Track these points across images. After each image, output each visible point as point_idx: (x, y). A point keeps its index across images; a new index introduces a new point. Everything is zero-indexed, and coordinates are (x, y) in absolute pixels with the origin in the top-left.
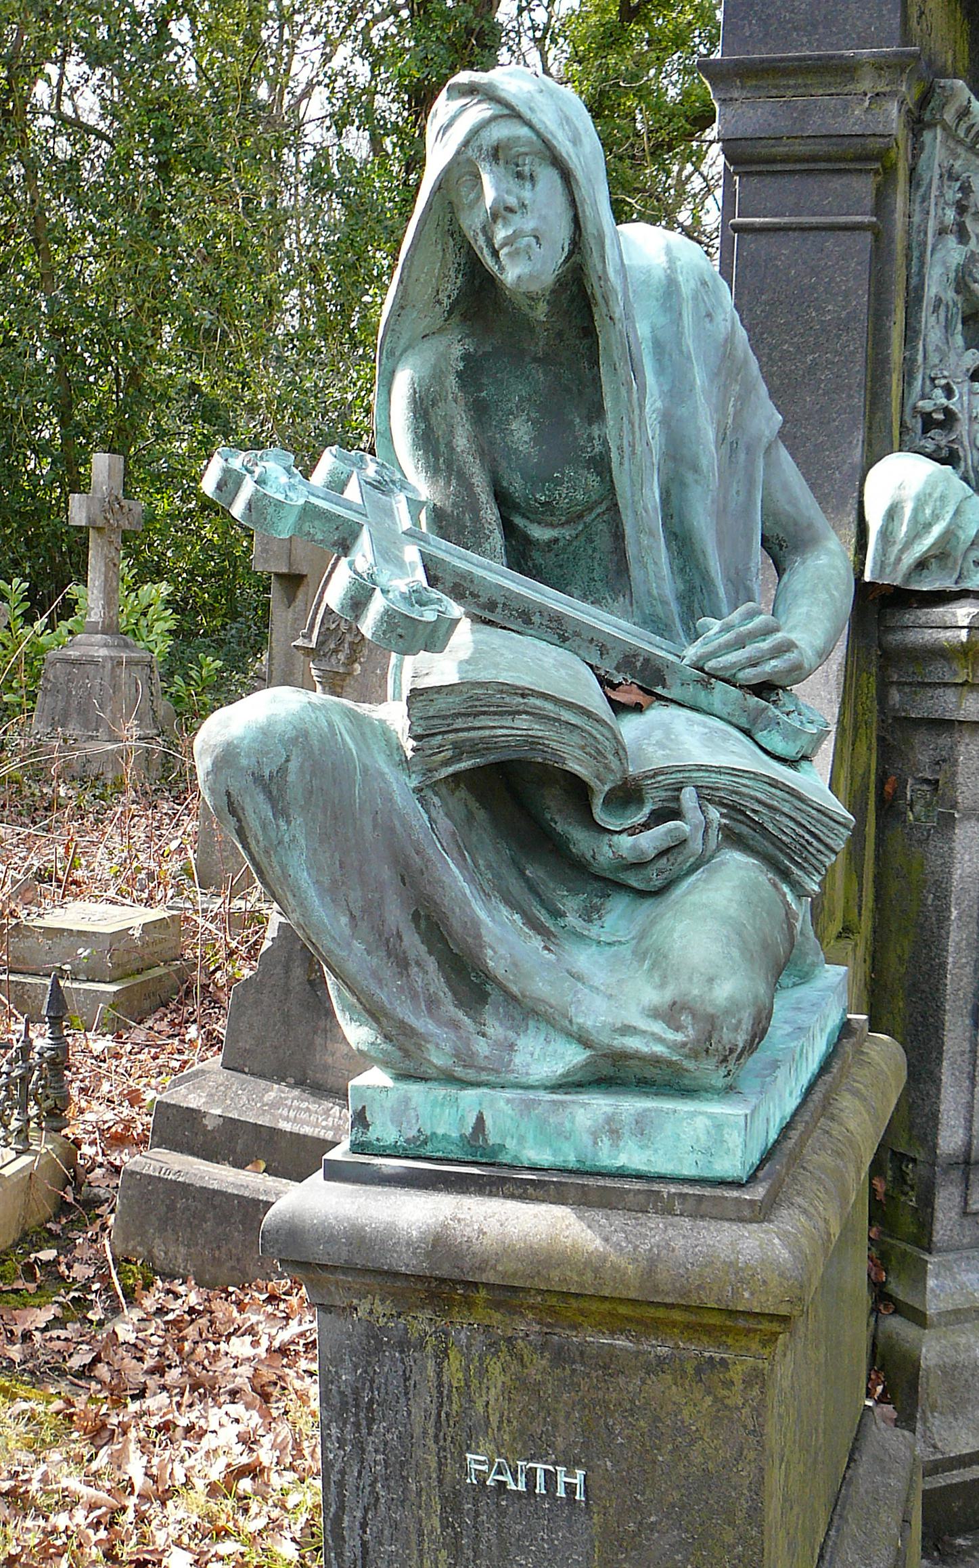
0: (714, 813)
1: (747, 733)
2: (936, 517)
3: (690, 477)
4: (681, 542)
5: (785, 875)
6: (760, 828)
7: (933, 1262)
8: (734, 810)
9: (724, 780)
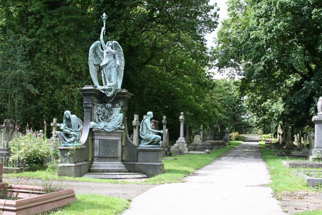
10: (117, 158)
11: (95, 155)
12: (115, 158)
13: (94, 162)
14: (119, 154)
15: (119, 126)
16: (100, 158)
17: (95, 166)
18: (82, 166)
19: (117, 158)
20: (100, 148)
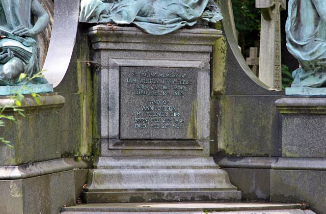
0: (12, 52)
1: (21, 43)
2: (92, 9)
3: (15, 6)
4: (15, 15)
5: (23, 60)
6: (19, 54)
7: (100, 158)
8: (15, 52)
9: (13, 48)
10: (193, 142)
11: (104, 133)
12: (185, 145)
13: (101, 162)
14: (204, 130)
15: (198, 12)
16: (125, 144)
17: (104, 178)
18: (54, 180)
19: (193, 142)
20: (126, 100)
